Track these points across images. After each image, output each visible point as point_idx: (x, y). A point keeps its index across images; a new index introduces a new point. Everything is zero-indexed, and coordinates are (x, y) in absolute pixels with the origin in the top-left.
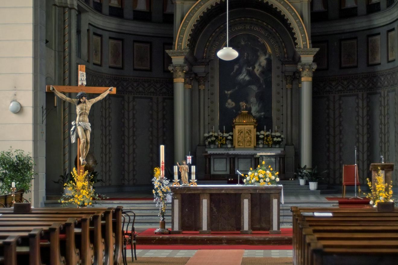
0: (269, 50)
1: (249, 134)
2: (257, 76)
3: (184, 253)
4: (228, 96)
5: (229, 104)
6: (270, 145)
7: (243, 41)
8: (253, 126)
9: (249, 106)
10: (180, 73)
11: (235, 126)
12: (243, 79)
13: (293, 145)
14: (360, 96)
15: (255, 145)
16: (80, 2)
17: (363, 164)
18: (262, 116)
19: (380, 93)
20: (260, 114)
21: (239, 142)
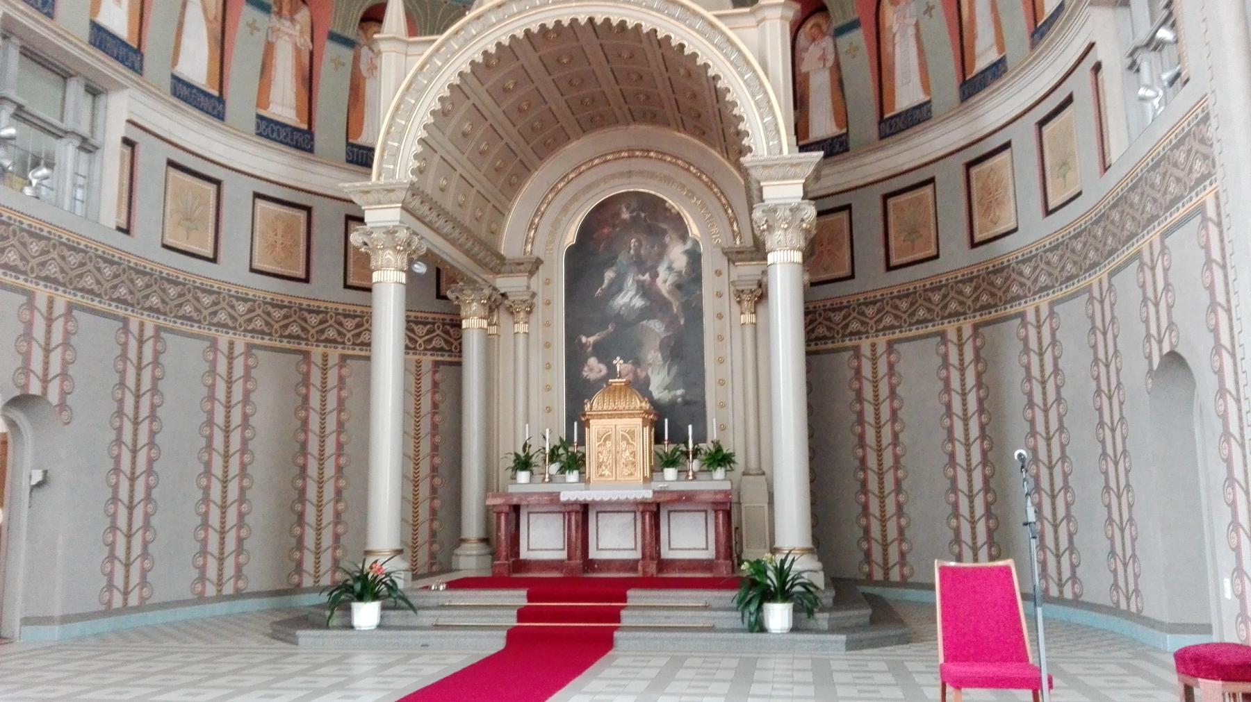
0: (694, 230)
1: (628, 443)
2: (664, 298)
3: (650, 664)
4: (590, 349)
5: (591, 370)
6: (691, 474)
7: (627, 208)
8: (639, 421)
9: (642, 374)
10: (389, 255)
11: (588, 420)
12: (627, 305)
13: (763, 474)
14: (952, 336)
15: (648, 474)
16: (12, 5)
17: (973, 529)
18: (679, 400)
19: (1022, 315)
20: (672, 393)
21: (600, 465)
